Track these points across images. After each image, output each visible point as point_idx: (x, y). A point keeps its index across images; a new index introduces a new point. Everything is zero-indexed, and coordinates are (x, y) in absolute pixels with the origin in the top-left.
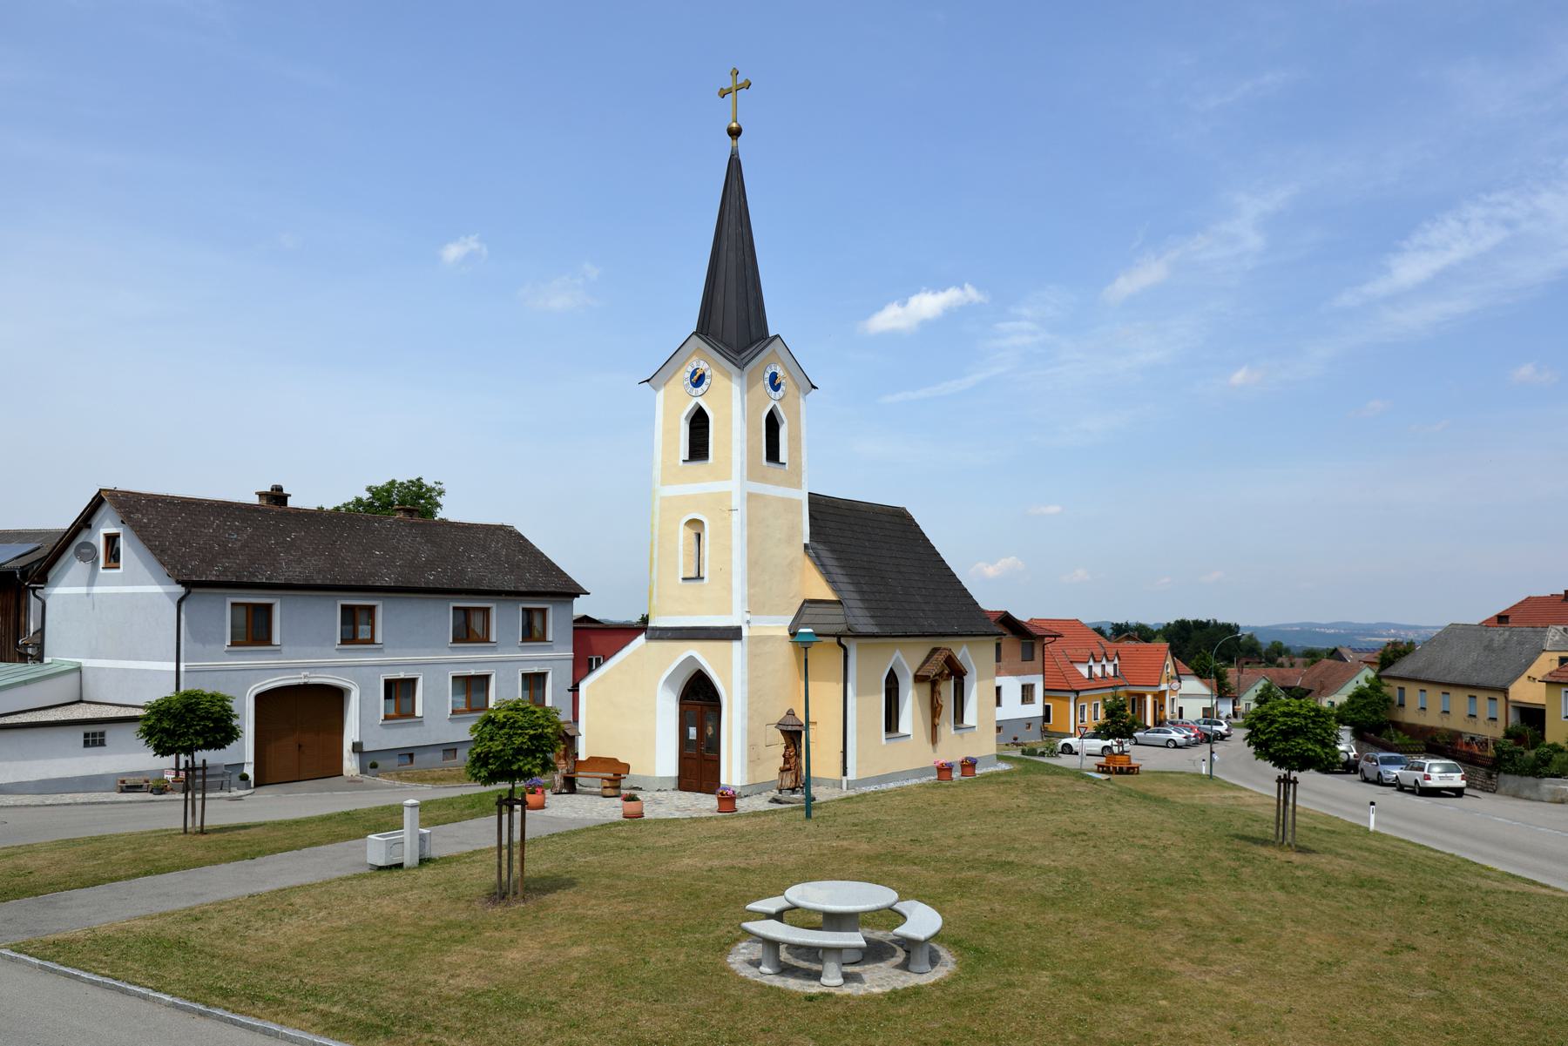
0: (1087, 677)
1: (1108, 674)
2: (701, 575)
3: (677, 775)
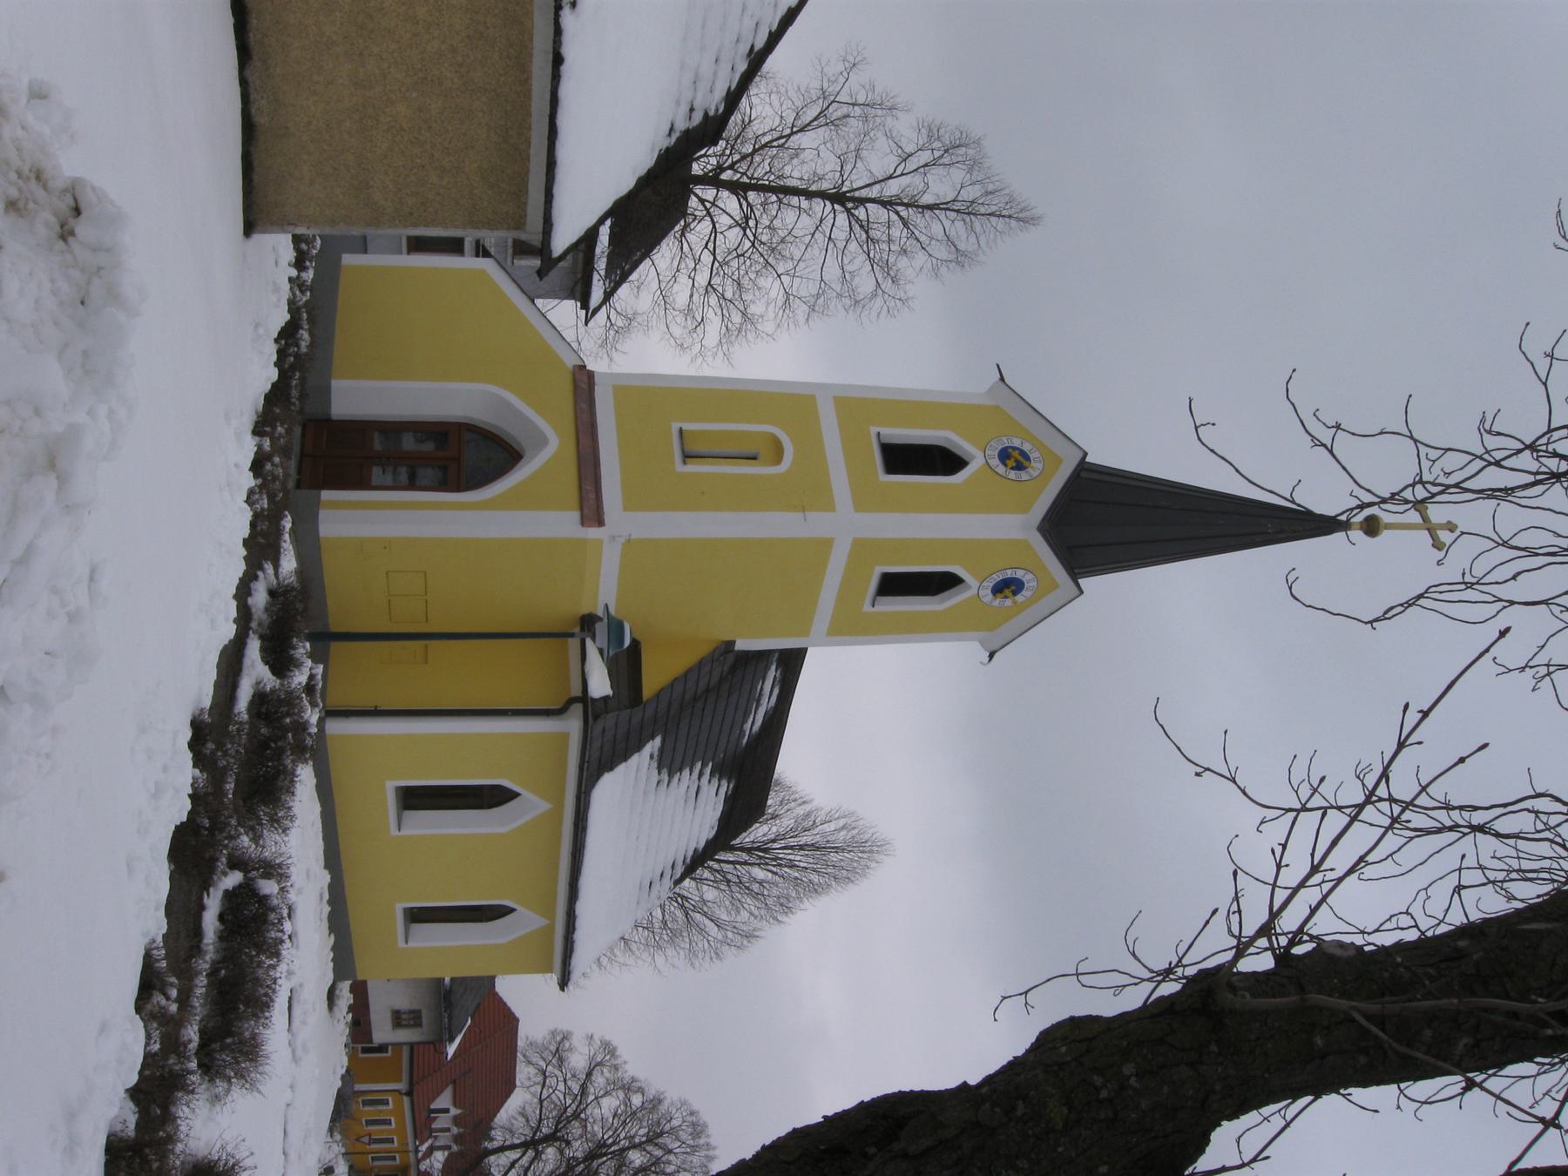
0: (433, 1126)
1: (435, 1118)
2: (688, 460)
3: (334, 417)
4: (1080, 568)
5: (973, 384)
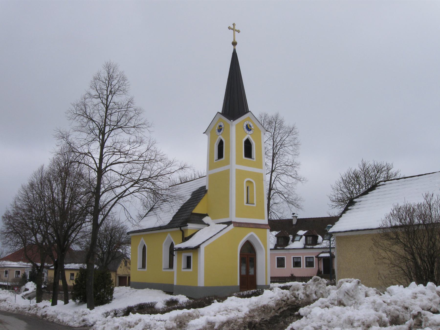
4: (244, 111)
5: (205, 139)
